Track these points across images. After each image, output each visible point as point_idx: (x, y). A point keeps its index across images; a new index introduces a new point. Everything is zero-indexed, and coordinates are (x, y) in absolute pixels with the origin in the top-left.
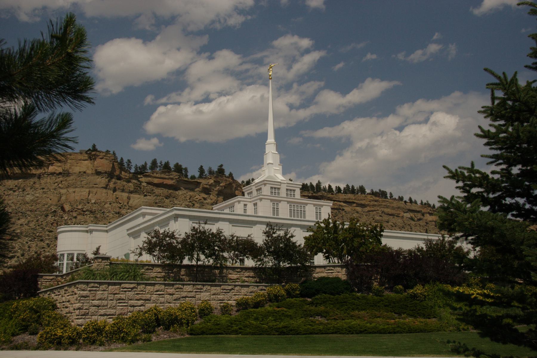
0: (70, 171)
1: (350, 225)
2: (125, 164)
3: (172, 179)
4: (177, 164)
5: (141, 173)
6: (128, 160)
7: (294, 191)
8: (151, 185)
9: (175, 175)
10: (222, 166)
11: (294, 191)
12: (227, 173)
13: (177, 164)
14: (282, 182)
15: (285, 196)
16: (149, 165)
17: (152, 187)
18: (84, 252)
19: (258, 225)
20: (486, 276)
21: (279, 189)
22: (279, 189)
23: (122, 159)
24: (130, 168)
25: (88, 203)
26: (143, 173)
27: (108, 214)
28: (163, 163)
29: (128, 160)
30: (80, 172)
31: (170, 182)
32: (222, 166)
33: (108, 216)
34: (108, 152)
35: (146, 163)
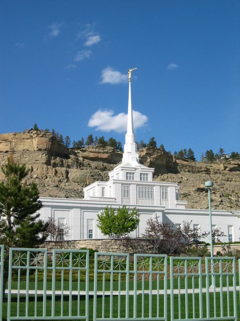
0: (15, 149)
1: (118, 213)
2: (64, 140)
3: (107, 153)
4: (112, 138)
5: (79, 148)
6: (67, 136)
7: (147, 174)
8: (88, 159)
9: (109, 149)
10: (153, 139)
11: (147, 174)
12: (158, 146)
13: (112, 138)
14: (136, 167)
15: (140, 181)
16: (85, 141)
17: (88, 161)
18: (177, 201)
19: (73, 209)
20: (132, 252)
21: (134, 173)
22: (134, 173)
23: (61, 136)
24: (69, 144)
25: (32, 178)
26: (80, 148)
27: (48, 187)
28: (98, 138)
29: (67, 136)
30: (24, 150)
31: (105, 156)
32: (153, 139)
33: (48, 189)
34: (47, 131)
35: (83, 139)
